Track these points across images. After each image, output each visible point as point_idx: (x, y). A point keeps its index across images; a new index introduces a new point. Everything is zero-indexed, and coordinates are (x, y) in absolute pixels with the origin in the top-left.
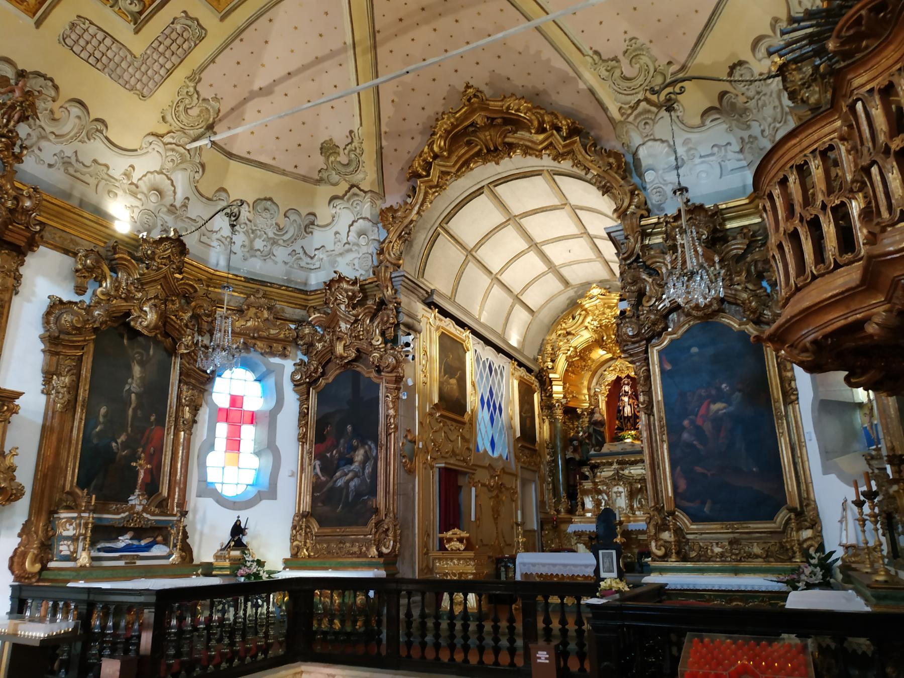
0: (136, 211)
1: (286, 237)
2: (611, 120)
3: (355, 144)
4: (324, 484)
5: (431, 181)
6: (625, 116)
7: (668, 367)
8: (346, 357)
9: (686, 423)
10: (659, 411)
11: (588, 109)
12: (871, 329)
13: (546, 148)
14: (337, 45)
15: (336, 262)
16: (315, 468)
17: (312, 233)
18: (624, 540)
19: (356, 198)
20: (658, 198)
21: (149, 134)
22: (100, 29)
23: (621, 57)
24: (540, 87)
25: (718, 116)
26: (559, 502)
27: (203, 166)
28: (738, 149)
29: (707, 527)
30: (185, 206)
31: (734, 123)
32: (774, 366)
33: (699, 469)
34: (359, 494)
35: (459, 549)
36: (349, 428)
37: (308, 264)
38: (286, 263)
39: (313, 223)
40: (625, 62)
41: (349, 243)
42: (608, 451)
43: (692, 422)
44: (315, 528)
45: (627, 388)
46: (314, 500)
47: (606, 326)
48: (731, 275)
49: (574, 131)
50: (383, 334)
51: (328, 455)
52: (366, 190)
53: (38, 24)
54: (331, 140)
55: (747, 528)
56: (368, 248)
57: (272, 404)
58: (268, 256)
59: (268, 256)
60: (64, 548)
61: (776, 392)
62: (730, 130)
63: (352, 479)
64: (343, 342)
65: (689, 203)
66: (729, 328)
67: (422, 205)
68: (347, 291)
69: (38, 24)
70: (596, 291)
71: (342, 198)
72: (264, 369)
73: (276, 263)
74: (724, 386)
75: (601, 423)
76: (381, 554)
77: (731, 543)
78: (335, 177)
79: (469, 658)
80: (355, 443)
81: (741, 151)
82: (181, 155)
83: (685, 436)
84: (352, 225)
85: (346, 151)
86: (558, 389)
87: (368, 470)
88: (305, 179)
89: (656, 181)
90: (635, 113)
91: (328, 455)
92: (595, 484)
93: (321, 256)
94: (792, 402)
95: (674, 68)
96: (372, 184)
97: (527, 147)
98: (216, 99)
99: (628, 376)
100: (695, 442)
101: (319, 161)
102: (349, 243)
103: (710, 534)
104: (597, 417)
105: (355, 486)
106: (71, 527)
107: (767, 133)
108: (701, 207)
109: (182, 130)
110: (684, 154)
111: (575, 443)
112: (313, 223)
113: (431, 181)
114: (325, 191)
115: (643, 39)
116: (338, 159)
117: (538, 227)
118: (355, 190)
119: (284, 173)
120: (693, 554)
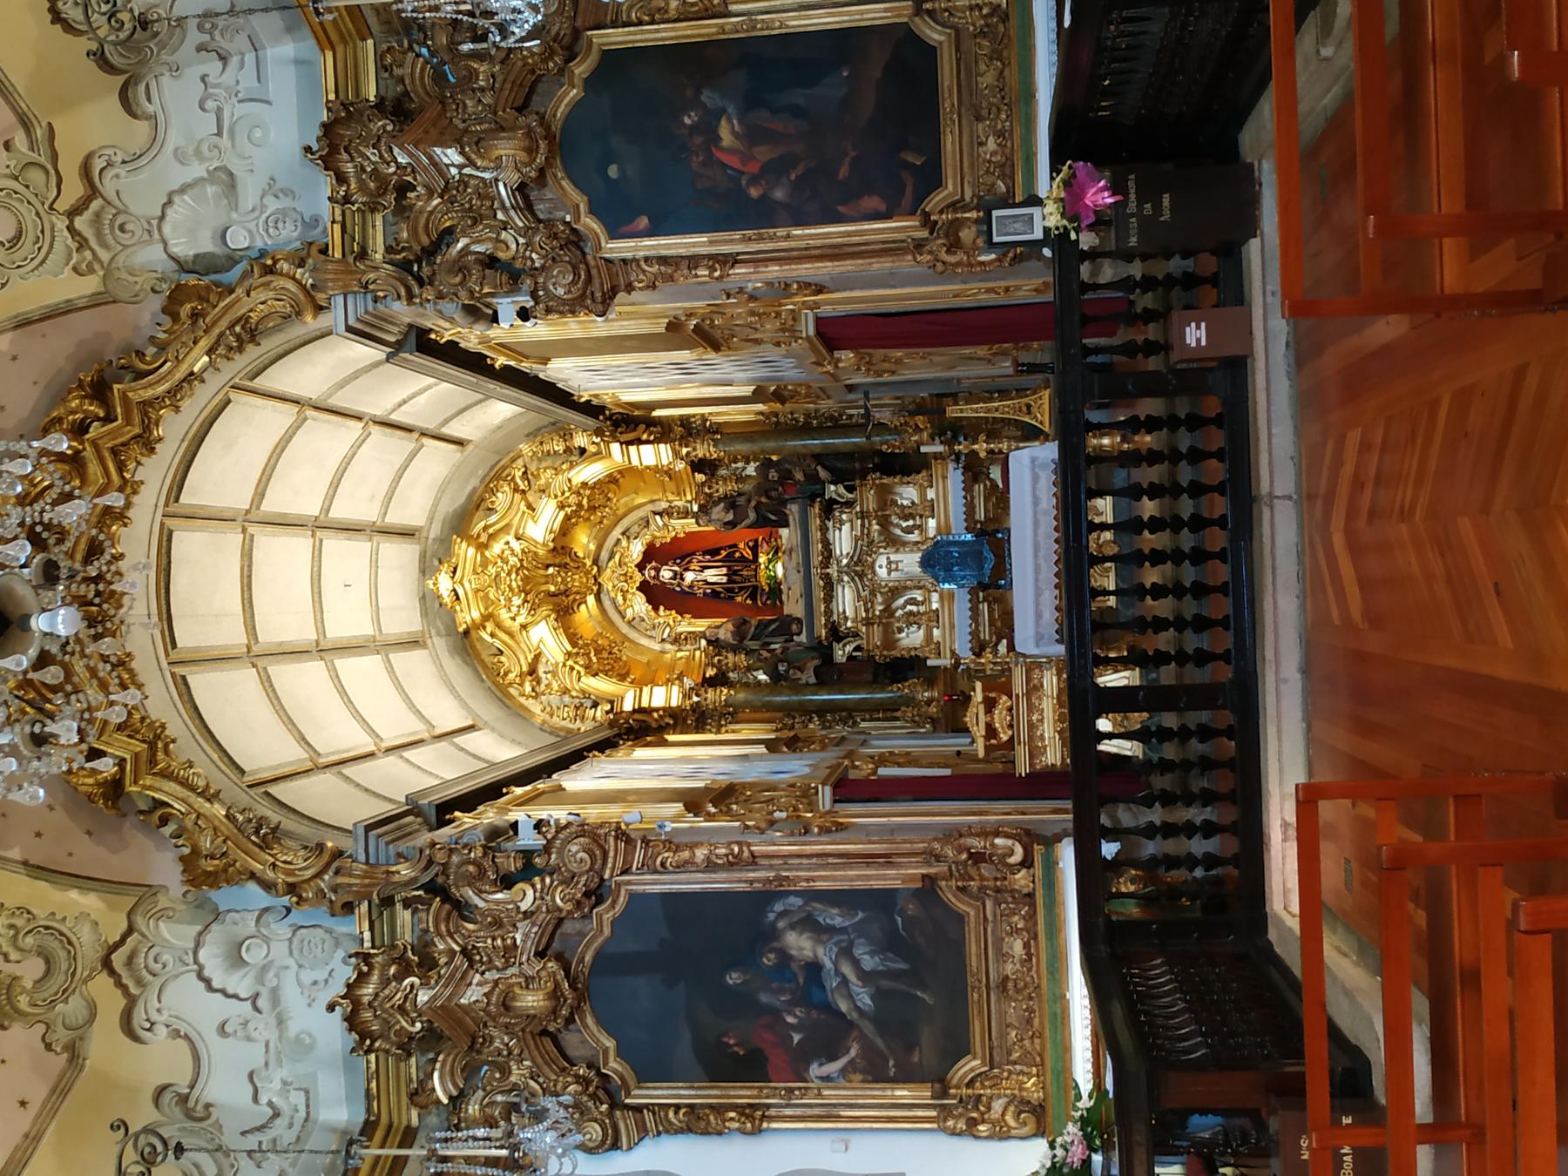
2: (97, 302)
4: (867, 1048)
5: (137, 756)
6: (96, 266)
7: (643, 222)
8: (557, 985)
10: (730, 242)
11: (55, 350)
13: (121, 468)
15: (298, 1039)
16: (826, 1079)
17: (208, 1106)
18: (982, 437)
19: (140, 960)
20: (290, 226)
21: (134, 115)
25: (142, 88)
26: (910, 701)
28: (220, 64)
29: (949, 162)
31: (164, 57)
32: (657, 31)
33: (843, 172)
34: (890, 943)
35: (1010, 709)
36: (733, 978)
37: (291, 1125)
39: (184, 1099)
41: (255, 998)
42: (801, 602)
43: (754, 180)
44: (970, 1066)
45: (666, 574)
46: (905, 1076)
47: (526, 579)
48: (473, 90)
49: (99, 390)
50: (507, 882)
51: (796, 1038)
52: (124, 926)
55: (950, 91)
62: (176, 69)
63: (856, 963)
64: (517, 990)
65: (315, 147)
66: (577, 106)
67: (193, 789)
68: (385, 982)
70: (444, 583)
71: (132, 1001)
74: (687, 121)
75: (740, 633)
76: (1027, 863)
77: (979, 119)
78: (73, 1008)
79: (1214, 449)
80: (769, 960)
81: (224, 59)
83: (779, 194)
85: (14, 956)
86: (660, 697)
87: (834, 917)
88: (60, 1090)
89: (252, 226)
90: (93, 243)
91: (796, 1038)
92: (868, 622)
93: (277, 1085)
95: (20, 141)
96: (112, 907)
99: (641, 567)
100: (793, 177)
102: (255, 998)
103: (995, 1017)
104: (725, 634)
105: (872, 953)
108: (327, 128)
110: (204, 166)
111: (781, 668)
112: (184, 1099)
113: (137, 756)
114: (104, 1042)
116: (29, 984)
117: (297, 493)
118: (118, 959)
119: (32, 1140)
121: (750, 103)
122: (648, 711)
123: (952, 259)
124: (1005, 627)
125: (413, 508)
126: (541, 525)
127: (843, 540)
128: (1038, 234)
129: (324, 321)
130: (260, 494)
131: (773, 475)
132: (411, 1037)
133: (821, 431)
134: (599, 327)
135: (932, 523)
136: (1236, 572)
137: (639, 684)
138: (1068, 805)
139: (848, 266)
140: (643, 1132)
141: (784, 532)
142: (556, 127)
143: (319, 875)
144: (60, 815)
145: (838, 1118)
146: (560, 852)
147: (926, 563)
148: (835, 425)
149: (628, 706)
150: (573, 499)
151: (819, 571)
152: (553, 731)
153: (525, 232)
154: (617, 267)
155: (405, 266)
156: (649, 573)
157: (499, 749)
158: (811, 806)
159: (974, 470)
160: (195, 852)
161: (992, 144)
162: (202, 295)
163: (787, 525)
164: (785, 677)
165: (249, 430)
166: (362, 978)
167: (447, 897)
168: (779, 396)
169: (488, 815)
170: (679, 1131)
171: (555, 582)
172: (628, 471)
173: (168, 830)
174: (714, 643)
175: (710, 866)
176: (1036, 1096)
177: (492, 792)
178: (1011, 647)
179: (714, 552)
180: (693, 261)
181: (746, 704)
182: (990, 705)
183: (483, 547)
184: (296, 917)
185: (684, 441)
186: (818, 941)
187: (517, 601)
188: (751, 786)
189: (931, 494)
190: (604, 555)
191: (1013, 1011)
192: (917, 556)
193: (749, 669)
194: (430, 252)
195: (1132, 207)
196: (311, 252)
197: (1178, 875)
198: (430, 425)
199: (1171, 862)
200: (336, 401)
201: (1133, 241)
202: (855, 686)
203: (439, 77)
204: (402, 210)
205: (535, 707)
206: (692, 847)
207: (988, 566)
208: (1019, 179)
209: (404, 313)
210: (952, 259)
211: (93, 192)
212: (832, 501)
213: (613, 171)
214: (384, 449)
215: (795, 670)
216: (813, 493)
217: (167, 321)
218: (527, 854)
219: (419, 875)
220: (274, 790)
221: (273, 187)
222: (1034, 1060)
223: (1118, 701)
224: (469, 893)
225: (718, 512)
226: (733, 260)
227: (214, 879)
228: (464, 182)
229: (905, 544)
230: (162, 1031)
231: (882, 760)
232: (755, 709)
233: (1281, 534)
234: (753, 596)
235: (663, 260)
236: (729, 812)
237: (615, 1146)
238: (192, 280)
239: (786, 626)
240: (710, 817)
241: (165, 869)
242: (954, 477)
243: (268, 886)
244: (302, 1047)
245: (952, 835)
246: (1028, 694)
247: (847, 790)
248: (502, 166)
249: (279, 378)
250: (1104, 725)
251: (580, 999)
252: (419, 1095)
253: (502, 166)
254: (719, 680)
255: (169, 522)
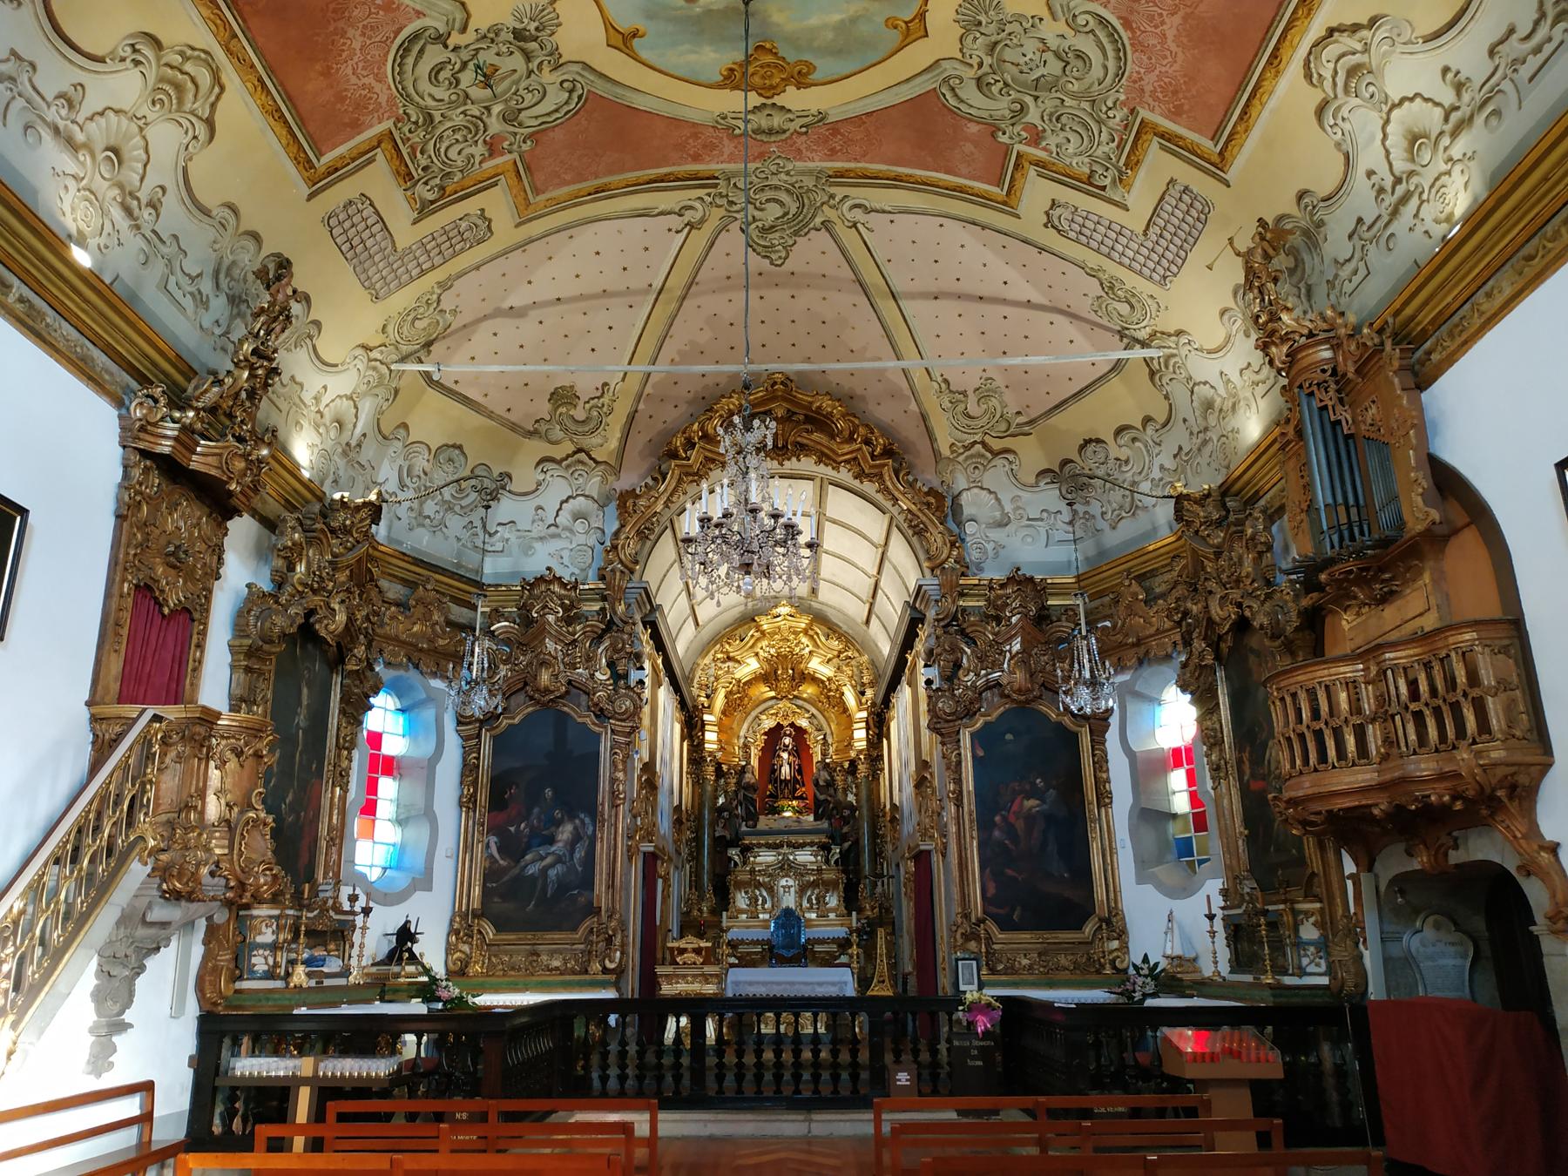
0: (316, 451)
1: (464, 503)
2: (936, 454)
3: (605, 400)
4: (504, 870)
7: (981, 753)
9: (997, 818)
10: (969, 803)
11: (910, 431)
12: (1376, 811)
14: (637, 283)
15: (531, 547)
16: (488, 846)
22: (377, 213)
23: (970, 393)
24: (859, 391)
26: (701, 898)
27: (397, 391)
30: (359, 445)
33: (1009, 872)
34: (563, 887)
36: (548, 793)
38: (459, 539)
39: (503, 488)
40: (972, 399)
43: (1004, 819)
44: (490, 931)
45: (787, 741)
49: (888, 452)
53: (311, 197)
54: (572, 387)
56: (584, 537)
57: (428, 748)
58: (439, 527)
59: (439, 527)
60: (260, 962)
61: (1091, 795)
63: (552, 866)
66: (1046, 717)
68: (561, 598)
69: (311, 197)
70: (784, 610)
71: (559, 462)
72: (424, 696)
73: (446, 538)
75: (750, 787)
76: (605, 970)
77: (1040, 954)
78: (557, 433)
80: (558, 814)
81: (1071, 523)
82: (381, 376)
83: (997, 833)
84: (566, 501)
86: (711, 736)
87: (579, 854)
88: (514, 427)
92: (752, 872)
93: (507, 535)
94: (1105, 805)
95: (1021, 419)
96: (611, 453)
97: (823, 454)
98: (454, 312)
99: (792, 725)
101: (544, 408)
103: (517, 946)
106: (270, 930)
107: (1108, 516)
108: (1031, 579)
109: (396, 345)
112: (503, 488)
114: (539, 448)
115: (1000, 382)
118: (582, 456)
119: (490, 415)
120: (1000, 967)
121: (1049, 818)
122: (703, 730)
123: (958, 936)
124: (746, 962)
125: (829, 597)
126: (816, 666)
127: (805, 857)
128: (962, 988)
129: (927, 572)
130: (834, 522)
131: (846, 813)
132: (529, 611)
133: (873, 843)
134: (924, 721)
135: (814, 916)
136: (768, 1099)
137: (720, 724)
138: (636, 996)
139: (956, 873)
140: (465, 739)
141: (811, 818)
142: (1034, 705)
143: (621, 562)
144: (661, 426)
145: (465, 853)
146: (626, 695)
147: (788, 912)
148: (877, 854)
149: (706, 717)
150: (833, 687)
151: (786, 839)
152: (693, 670)
153: (974, 685)
154: (954, 737)
155: (955, 618)
156: (788, 730)
157: (683, 643)
158: (642, 839)
159: (844, 944)
160: (638, 497)
161: (1025, 962)
162: (940, 507)
163: (816, 819)
164: (720, 816)
165: (872, 522)
166: (564, 585)
167: (604, 631)
168: (893, 820)
169: (648, 648)
170: (464, 759)
171: (784, 673)
172: (850, 722)
173: (649, 481)
174: (743, 770)
175: (613, 781)
176: (471, 972)
177: (660, 646)
178: (732, 966)
179: (800, 771)
180: (958, 781)
181: (703, 789)
182: (698, 951)
183: (805, 632)
184: (599, 548)
185: (868, 756)
186: (566, 843)
187: (773, 651)
188: (655, 800)
189: (832, 916)
190: (800, 702)
191: (519, 959)
192: (792, 905)
193: (726, 792)
194: (962, 632)
195: (976, 1043)
196: (964, 568)
197: (595, 1059)
198: (876, 609)
199: (605, 1055)
200: (887, 564)
201: (956, 1043)
202: (712, 862)
203: (1061, 641)
204: (987, 618)
205: (707, 660)
206: (625, 771)
207: (784, 952)
208: (1004, 978)
209: (931, 614)
210: (958, 936)
211: (995, 454)
212: (829, 850)
213: (1009, 737)
214: (864, 586)
215: (724, 822)
216: (835, 837)
217: (925, 489)
218: (626, 676)
219: (616, 615)
220: (668, 531)
221: (999, 547)
222: (490, 971)
223: (698, 1029)
224: (607, 643)
225: (825, 775)
226: (959, 804)
227: (622, 506)
228: (1002, 653)
229: (801, 898)
230: (541, 477)
231: (666, 880)
232: (701, 796)
233: (788, 1126)
234: (771, 796)
235: (959, 763)
236: (641, 788)
237: (459, 723)
238: (948, 502)
239: (752, 817)
240: (640, 778)
241: (627, 481)
242: (841, 932)
243: (616, 534)
244: (527, 550)
245: (623, 926)
246: (703, 975)
247: (651, 860)
248: (1009, 673)
249: (896, 538)
250: (684, 1021)
251: (543, 705)
252: (496, 614)
253: (1009, 673)
254: (719, 772)
255: (818, 481)
